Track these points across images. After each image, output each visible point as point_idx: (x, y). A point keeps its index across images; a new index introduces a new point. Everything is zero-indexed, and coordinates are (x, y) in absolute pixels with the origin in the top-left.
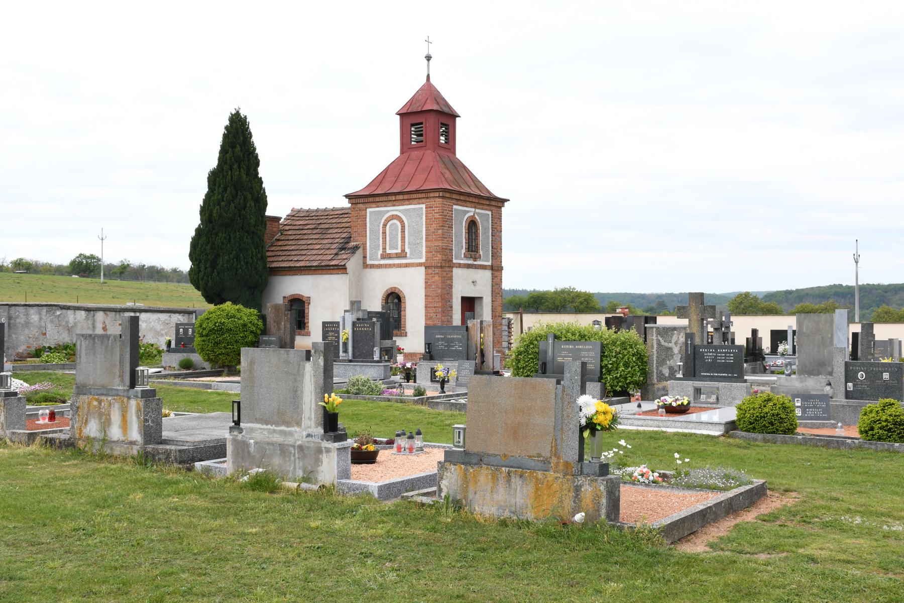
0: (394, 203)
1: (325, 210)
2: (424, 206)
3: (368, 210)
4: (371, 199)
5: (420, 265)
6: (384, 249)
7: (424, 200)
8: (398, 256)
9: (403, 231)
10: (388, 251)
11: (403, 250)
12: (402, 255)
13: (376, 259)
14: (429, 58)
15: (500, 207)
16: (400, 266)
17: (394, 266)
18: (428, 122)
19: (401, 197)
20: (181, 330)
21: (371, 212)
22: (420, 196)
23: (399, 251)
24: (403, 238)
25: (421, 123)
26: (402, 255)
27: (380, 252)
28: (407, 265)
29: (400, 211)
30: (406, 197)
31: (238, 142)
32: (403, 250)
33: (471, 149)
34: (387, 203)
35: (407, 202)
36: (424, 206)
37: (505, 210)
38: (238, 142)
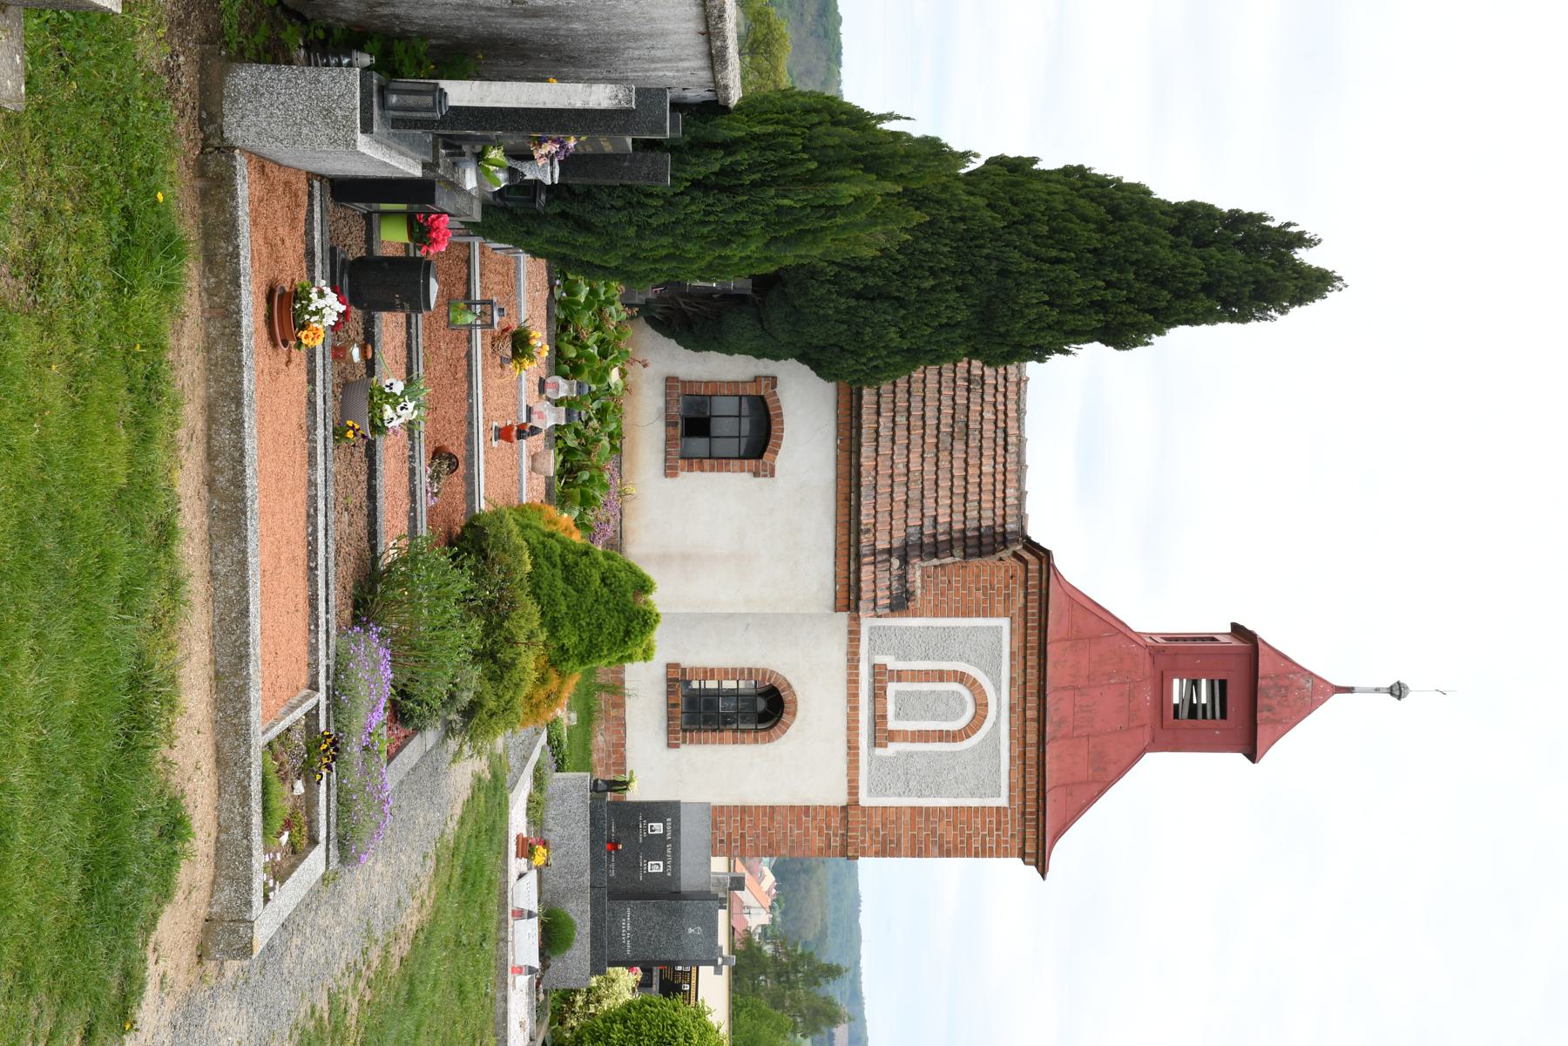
0: (1018, 710)
1: (1021, 466)
2: (1002, 801)
4: (1033, 639)
5: (853, 789)
6: (899, 676)
7: (1018, 802)
8: (878, 719)
9: (943, 736)
10: (892, 688)
11: (892, 736)
13: (873, 650)
14: (1398, 691)
15: (1023, 855)
16: (852, 727)
17: (853, 696)
18: (1235, 694)
19: (1032, 738)
20: (658, 828)
21: (998, 630)
23: (893, 724)
24: (924, 736)
25: (1224, 716)
26: (881, 735)
27: (893, 663)
28: (852, 748)
29: (996, 724)
30: (1032, 752)
31: (1237, 267)
32: (892, 736)
33: (1169, 795)
34: (1020, 687)
35: (1018, 750)
36: (1002, 801)
37: (1014, 870)
38: (1237, 267)
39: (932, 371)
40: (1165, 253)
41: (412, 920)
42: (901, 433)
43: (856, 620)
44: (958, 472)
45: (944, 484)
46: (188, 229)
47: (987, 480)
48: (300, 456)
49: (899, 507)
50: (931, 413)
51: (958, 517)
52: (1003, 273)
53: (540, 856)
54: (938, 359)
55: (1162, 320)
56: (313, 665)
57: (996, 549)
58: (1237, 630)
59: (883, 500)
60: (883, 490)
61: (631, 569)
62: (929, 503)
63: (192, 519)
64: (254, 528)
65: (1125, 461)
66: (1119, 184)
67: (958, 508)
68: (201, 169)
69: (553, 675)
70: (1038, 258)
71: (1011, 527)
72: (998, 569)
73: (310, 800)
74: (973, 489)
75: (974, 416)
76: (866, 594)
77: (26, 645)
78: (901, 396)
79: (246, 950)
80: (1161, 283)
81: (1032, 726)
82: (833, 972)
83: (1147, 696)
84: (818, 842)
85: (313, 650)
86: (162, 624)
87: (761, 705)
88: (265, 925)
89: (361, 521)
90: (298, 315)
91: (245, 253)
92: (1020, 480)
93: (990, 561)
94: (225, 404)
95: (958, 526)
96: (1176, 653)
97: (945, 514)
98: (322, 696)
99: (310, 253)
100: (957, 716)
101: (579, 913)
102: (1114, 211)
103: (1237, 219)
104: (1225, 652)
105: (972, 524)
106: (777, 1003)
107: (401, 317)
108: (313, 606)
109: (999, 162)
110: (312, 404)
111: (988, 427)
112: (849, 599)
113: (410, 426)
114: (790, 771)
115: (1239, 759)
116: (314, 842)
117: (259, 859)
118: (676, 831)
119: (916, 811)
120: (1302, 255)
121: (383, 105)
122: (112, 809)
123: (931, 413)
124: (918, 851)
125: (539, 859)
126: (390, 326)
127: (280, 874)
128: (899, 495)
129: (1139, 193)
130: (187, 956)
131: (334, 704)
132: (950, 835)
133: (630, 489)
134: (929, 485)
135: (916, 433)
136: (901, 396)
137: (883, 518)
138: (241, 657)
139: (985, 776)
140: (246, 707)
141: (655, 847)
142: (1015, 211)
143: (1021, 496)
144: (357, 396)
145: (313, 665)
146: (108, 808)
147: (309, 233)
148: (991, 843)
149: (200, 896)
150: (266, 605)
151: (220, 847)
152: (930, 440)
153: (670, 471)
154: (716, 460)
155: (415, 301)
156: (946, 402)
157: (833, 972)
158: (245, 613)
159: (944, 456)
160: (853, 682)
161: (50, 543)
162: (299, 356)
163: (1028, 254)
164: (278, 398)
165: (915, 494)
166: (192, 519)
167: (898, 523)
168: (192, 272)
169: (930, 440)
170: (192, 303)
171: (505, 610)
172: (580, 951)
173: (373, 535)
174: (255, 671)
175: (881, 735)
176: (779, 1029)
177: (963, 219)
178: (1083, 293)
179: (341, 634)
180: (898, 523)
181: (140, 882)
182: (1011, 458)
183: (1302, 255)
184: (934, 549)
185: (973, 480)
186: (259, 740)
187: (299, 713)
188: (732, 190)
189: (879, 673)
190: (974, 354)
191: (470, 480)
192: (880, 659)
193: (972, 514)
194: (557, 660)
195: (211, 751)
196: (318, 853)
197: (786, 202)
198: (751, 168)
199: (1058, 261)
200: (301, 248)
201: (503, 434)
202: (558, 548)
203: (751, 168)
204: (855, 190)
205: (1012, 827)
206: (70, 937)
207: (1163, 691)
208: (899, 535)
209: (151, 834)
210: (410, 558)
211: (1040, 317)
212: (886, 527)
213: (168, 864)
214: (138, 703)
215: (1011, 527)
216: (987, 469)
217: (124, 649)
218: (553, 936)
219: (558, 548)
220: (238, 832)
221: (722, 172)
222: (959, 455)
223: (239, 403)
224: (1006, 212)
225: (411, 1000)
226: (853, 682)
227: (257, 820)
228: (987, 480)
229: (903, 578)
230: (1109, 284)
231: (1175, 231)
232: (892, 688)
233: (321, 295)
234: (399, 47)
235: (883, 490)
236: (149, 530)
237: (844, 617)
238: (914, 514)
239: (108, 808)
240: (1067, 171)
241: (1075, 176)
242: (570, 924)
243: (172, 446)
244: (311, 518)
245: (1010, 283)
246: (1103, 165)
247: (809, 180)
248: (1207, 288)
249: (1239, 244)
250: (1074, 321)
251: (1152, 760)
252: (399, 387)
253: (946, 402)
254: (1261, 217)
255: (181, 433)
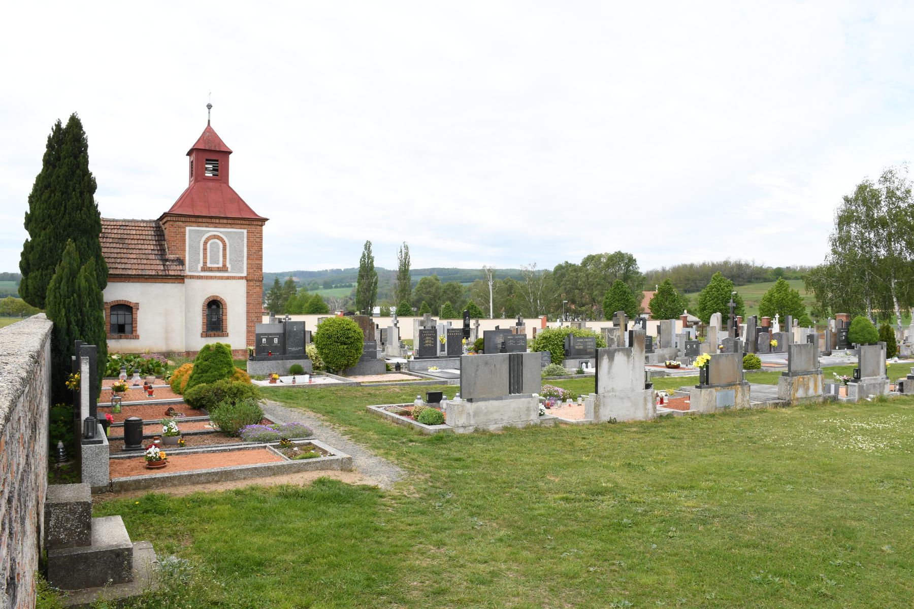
0: (216, 225)
2: (245, 231)
3: (188, 229)
4: (193, 219)
5: (241, 278)
6: (205, 263)
10: (209, 265)
12: (224, 269)
13: (196, 271)
14: (209, 107)
15: (262, 226)
17: (211, 278)
18: (210, 156)
19: (225, 221)
20: (264, 340)
22: (242, 222)
23: (221, 265)
27: (201, 265)
28: (228, 278)
30: (230, 221)
31: (67, 149)
32: (224, 265)
33: (241, 178)
34: (208, 224)
36: (245, 231)
37: (266, 228)
38: (67, 149)
39: (103, 250)
40: (63, 171)
41: (312, 414)
42: (123, 261)
43: (186, 276)
44: (136, 242)
45: (140, 247)
46: (142, 494)
47: (138, 232)
48: (195, 456)
49: (149, 262)
50: (115, 251)
51: (151, 242)
52: (70, 226)
53: (275, 376)
54: (100, 248)
55: (86, 174)
56: (258, 448)
57: (161, 230)
58: (189, 154)
59: (146, 267)
60: (143, 267)
61: (202, 351)
62: (147, 252)
63: (231, 486)
64: (228, 468)
65: (133, 187)
66: (36, 186)
67: (148, 242)
68: (119, 492)
69: (236, 375)
70: (64, 214)
71: (154, 225)
72: (169, 230)
73: (298, 445)
74: (141, 237)
75: (116, 236)
76: (179, 273)
77: (290, 526)
78: (110, 260)
79: (350, 459)
80: (73, 173)
81: (221, 221)
82: (277, 282)
83: (211, 184)
84: (258, 289)
85: (254, 448)
86: (266, 491)
87: (214, 307)
88: (340, 455)
89: (205, 437)
90: (157, 460)
91: (144, 477)
92: (138, 221)
93: (166, 232)
94: (192, 479)
95: (154, 242)
96: (197, 174)
97: (150, 246)
98: (268, 444)
99: (129, 458)
100: (218, 245)
101: (290, 363)
102: (48, 186)
103: (50, 145)
104: (197, 159)
105: (153, 238)
106: (286, 299)
107: (144, 427)
108: (241, 449)
109: (27, 226)
110: (178, 454)
111: (119, 231)
112: (180, 279)
113: (178, 422)
114: (235, 298)
115: (231, 156)
116: (310, 443)
117: (322, 458)
118: (265, 334)
119: (248, 258)
120: (64, 126)
121: (92, 437)
122: (323, 498)
123: (115, 251)
124: (261, 258)
125: (276, 376)
126: (147, 431)
127: (325, 452)
128: (145, 262)
129: (39, 178)
130: (352, 474)
131: (269, 441)
132: (255, 248)
133: (147, 351)
134: (141, 252)
135: (123, 255)
136: (110, 260)
137: (153, 267)
138: (269, 468)
139: (238, 236)
140: (283, 466)
141: (270, 340)
142: (47, 221)
143: (143, 221)
144: (167, 440)
145: (258, 448)
146: (324, 500)
147: (122, 458)
148: (258, 235)
149: (337, 473)
150: (248, 463)
151: (322, 469)
152: (125, 251)
153: (137, 337)
154: (133, 323)
155: (139, 424)
156: (111, 245)
157: (277, 282)
158: (255, 468)
159: (130, 246)
160: (207, 278)
161: (257, 523)
162: (170, 458)
163: (63, 217)
164: (180, 465)
165: (144, 257)
166: (231, 486)
167: (154, 262)
168: (157, 492)
169: (125, 251)
170: (165, 491)
171: (214, 391)
172: (302, 363)
173: (208, 433)
174: (272, 464)
175: (224, 269)
176: (295, 298)
177: (50, 239)
178: (77, 199)
179: (245, 440)
180: (154, 262)
181: (339, 489)
182: (130, 224)
183: (64, 126)
184: (162, 250)
185: (138, 237)
186: (290, 461)
187: (276, 450)
188: (83, 322)
189: (204, 269)
190: (97, 236)
191: (175, 403)
192: (199, 269)
193: (150, 237)
194: (231, 373)
195: (296, 475)
196: (312, 441)
197: (88, 304)
198: (76, 316)
199: (65, 207)
200: (128, 460)
201: (151, 394)
202: (196, 375)
203: (76, 316)
204: (83, 281)
205: (253, 229)
206: (361, 504)
207: (208, 179)
208: (158, 262)
209: (324, 488)
210: (216, 420)
211: (85, 214)
212: (157, 267)
213: (331, 482)
214: (289, 495)
215: (154, 225)
216: (134, 232)
217: (277, 501)
218: (297, 371)
219: (196, 375)
220: (318, 465)
221: (77, 325)
222: (130, 241)
223: (192, 475)
224: (48, 224)
225: (333, 413)
226: (207, 278)
227: (314, 460)
228: (138, 232)
229: (173, 261)
230: (74, 190)
231: (54, 167)
232: (209, 265)
233: (150, 453)
234: (54, 433)
235: (143, 267)
236: (239, 497)
237: (186, 280)
238: (151, 257)
239: (324, 500)
240: (31, 202)
241: (32, 199)
242: (294, 366)
243: (211, 493)
244: (214, 452)
245: (73, 224)
246: (29, 190)
247: (79, 296)
248: (76, 157)
249: (60, 146)
250: (87, 202)
251: (231, 184)
252: (166, 428)
253: (111, 245)
254: (49, 138)
255: (206, 491)
